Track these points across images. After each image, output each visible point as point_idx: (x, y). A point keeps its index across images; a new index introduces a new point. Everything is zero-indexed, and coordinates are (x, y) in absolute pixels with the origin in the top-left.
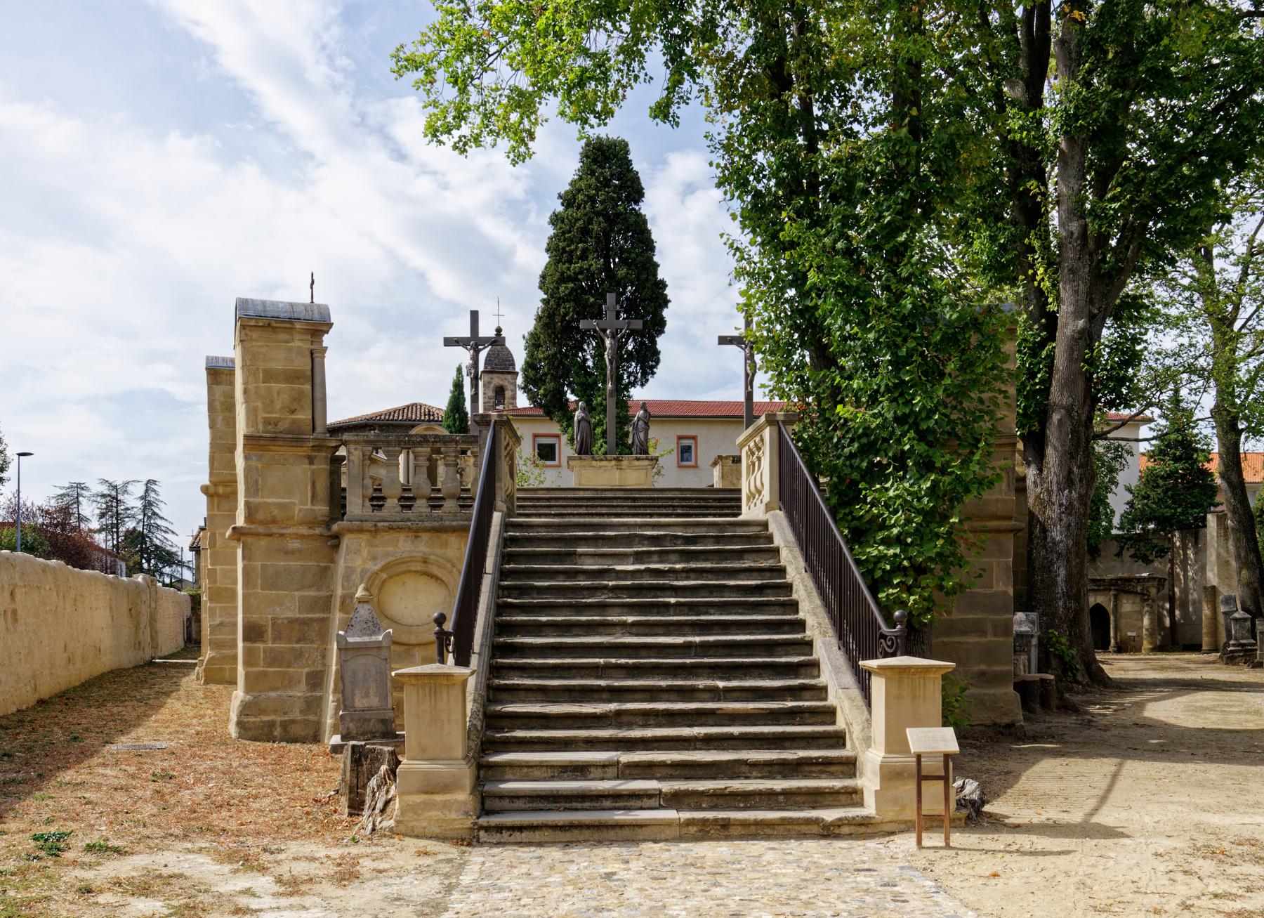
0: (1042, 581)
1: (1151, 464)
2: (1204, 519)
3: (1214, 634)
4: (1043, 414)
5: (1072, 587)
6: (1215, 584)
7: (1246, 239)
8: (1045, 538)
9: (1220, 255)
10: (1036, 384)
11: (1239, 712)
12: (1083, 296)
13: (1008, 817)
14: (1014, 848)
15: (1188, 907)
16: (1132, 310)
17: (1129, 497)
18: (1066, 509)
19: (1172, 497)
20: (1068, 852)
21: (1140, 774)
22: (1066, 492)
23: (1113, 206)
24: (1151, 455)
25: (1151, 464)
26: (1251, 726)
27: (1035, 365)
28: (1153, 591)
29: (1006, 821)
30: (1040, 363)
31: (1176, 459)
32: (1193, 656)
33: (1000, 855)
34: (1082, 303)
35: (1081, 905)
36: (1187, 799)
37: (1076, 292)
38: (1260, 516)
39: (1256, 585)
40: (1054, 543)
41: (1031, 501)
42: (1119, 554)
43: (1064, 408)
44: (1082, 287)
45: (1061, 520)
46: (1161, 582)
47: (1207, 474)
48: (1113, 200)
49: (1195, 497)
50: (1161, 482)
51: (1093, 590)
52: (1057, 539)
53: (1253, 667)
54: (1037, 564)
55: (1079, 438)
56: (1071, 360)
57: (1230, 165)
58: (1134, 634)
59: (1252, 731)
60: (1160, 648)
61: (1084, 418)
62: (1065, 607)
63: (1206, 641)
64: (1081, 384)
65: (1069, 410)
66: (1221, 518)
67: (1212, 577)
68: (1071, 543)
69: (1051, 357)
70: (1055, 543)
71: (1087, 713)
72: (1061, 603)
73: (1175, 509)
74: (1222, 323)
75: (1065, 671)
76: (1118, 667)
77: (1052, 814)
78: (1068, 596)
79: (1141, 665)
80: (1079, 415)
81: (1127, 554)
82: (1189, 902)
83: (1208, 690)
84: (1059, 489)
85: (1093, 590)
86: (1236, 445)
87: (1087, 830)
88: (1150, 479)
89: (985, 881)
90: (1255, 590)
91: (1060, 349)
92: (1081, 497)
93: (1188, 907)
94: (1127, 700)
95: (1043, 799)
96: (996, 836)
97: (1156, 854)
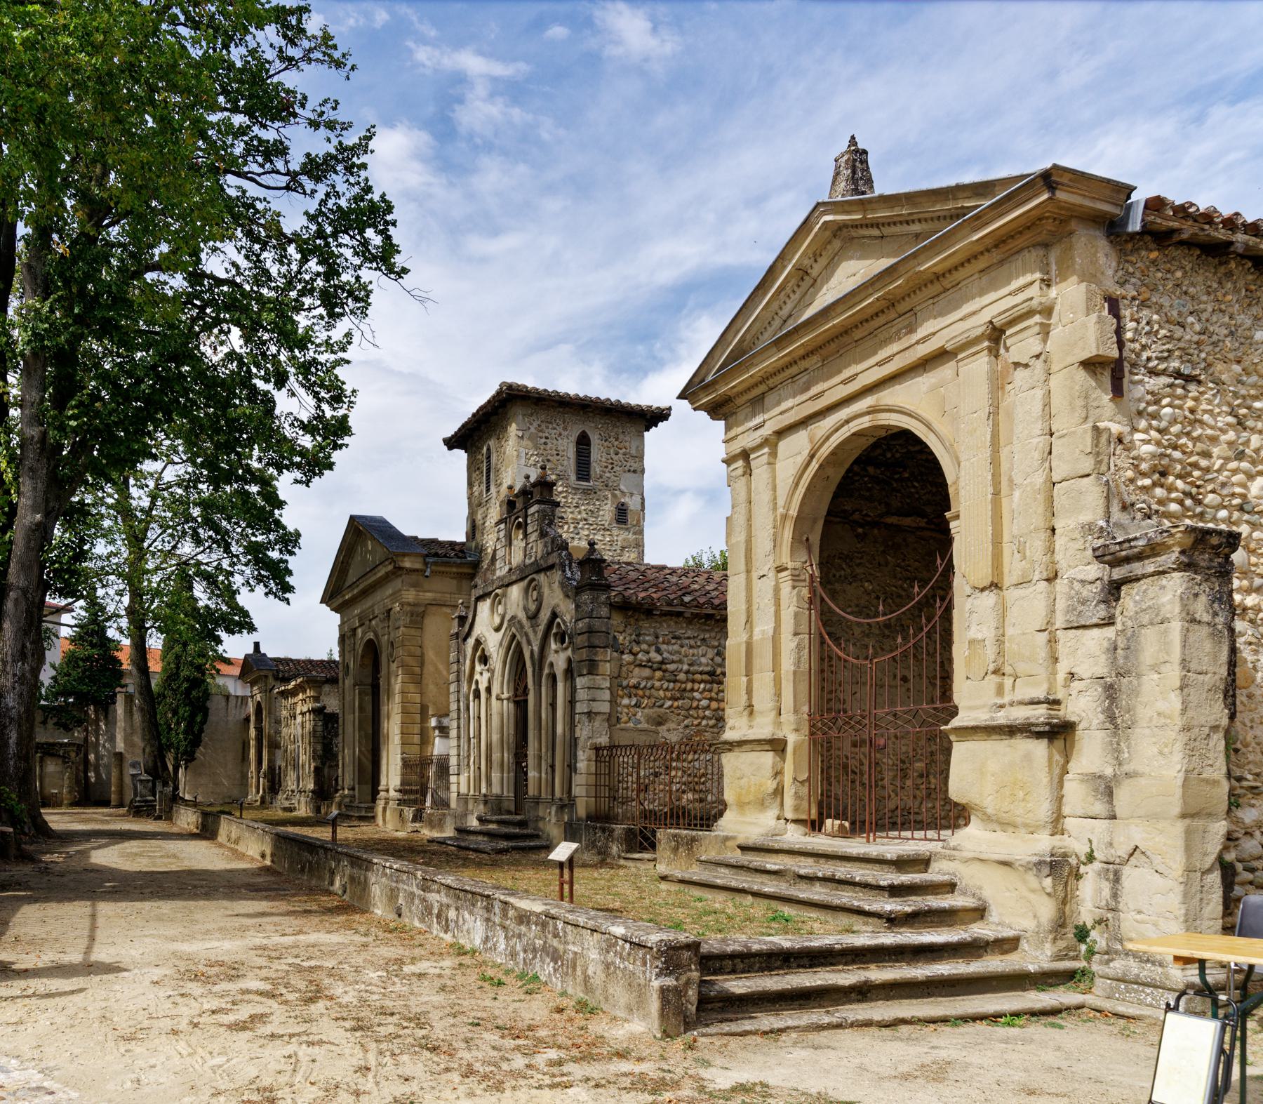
1: (72, 648)
3: (121, 791)
12: (40, 494)
13: (13, 963)
14: (30, 992)
15: (196, 1025)
16: (79, 516)
17: (54, 673)
20: (81, 990)
21: (110, 913)
24: (72, 640)
25: (72, 648)
28: (73, 755)
29: (14, 967)
31: (93, 646)
32: (105, 810)
33: (19, 1000)
34: (39, 500)
35: (109, 1036)
36: (155, 932)
37: (35, 489)
44: (40, 485)
46: (79, 747)
47: (117, 662)
50: (81, 663)
57: (160, 416)
60: (75, 804)
61: (37, 600)
62: (15, 767)
63: (114, 798)
65: (25, 592)
66: (129, 698)
67: (120, 746)
68: (22, 710)
71: (41, 861)
74: (136, 540)
76: (57, 820)
77: (47, 958)
79: (66, 818)
81: (51, 723)
82: (195, 1021)
84: (14, 661)
86: (143, 641)
87: (89, 968)
88: (71, 659)
89: (14, 1027)
93: (196, 1025)
94: (72, 849)
95: (35, 943)
96: (9, 983)
97: (153, 982)
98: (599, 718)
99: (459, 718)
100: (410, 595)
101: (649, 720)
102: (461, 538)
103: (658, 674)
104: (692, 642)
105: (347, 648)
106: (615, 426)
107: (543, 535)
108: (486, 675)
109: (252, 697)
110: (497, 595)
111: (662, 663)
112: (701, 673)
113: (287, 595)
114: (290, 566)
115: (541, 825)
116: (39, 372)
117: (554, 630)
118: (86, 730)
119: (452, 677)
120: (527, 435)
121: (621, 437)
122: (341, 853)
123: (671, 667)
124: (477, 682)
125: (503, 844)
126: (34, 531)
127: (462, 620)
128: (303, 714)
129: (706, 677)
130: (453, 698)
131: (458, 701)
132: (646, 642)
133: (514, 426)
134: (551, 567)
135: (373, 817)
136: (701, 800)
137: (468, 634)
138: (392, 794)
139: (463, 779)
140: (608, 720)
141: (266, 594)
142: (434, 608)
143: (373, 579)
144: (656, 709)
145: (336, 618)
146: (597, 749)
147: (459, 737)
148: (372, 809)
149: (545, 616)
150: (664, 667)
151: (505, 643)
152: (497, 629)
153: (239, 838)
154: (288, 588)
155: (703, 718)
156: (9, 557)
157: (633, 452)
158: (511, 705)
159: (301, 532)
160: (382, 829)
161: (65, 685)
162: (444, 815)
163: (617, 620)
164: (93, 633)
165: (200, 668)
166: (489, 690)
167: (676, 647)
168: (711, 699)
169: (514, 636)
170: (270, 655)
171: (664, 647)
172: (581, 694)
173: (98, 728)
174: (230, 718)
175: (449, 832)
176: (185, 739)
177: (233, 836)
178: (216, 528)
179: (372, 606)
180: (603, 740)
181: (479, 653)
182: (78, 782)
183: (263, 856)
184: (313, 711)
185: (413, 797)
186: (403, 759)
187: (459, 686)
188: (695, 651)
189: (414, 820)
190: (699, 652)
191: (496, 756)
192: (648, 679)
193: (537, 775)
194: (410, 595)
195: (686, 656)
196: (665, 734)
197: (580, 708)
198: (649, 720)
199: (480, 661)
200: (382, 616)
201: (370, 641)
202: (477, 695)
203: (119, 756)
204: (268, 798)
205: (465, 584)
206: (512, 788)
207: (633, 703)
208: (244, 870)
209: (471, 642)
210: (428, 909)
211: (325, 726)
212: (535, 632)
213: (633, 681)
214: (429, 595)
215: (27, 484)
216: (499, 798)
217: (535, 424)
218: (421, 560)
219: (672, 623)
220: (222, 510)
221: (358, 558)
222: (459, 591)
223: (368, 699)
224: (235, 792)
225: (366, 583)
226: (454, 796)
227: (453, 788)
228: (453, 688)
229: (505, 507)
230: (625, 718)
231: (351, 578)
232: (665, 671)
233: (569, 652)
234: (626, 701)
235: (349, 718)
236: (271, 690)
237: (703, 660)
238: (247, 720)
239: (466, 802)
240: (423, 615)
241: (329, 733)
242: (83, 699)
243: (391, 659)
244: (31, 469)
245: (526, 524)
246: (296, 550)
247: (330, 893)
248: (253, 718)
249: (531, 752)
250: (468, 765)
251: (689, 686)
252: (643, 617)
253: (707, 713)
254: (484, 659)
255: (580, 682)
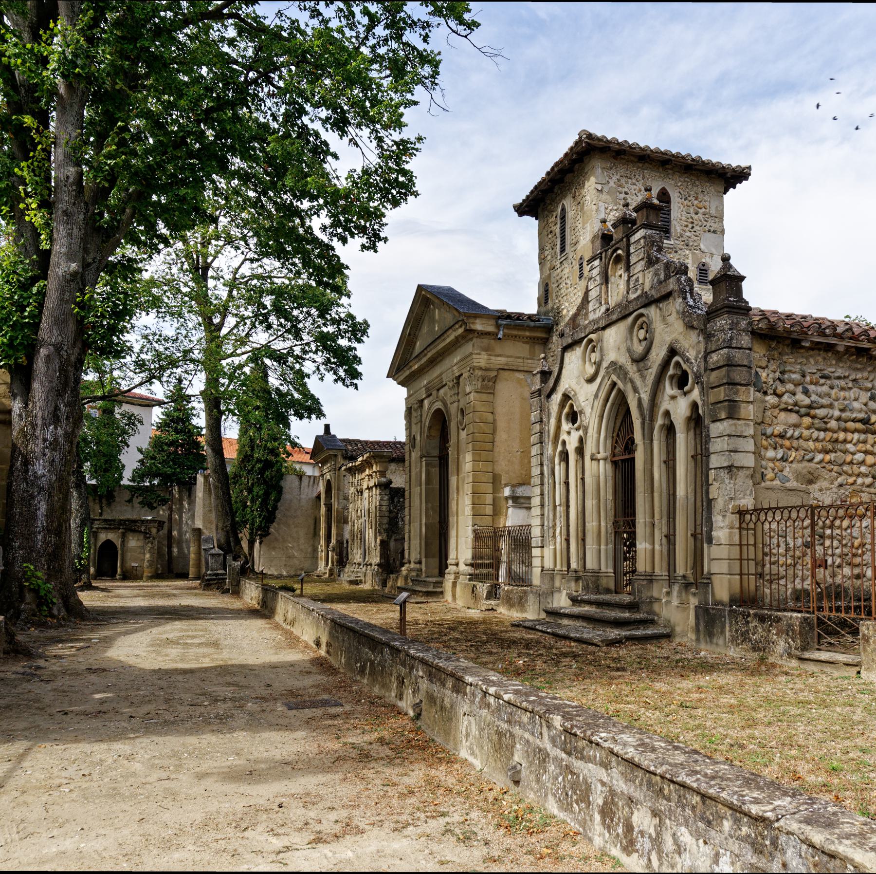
0: (21, 514)
1: (158, 433)
2: (195, 479)
4: (31, 349)
5: (52, 522)
6: (201, 527)
7: (231, 270)
8: (27, 471)
9: (212, 277)
10: (25, 317)
11: (200, 645)
17: (141, 457)
18: (51, 444)
19: (172, 460)
22: (51, 427)
23: (109, 162)
25: (158, 433)
26: (206, 663)
27: (25, 299)
28: (154, 531)
30: (30, 298)
31: (177, 432)
34: (75, 248)
37: (70, 235)
38: (234, 478)
39: (229, 528)
40: (36, 477)
41: (15, 433)
42: (130, 501)
43: (53, 345)
45: (44, 455)
46: (161, 524)
47: (197, 445)
48: (109, 156)
49: (190, 461)
50: (166, 448)
51: (105, 528)
52: (40, 473)
53: (223, 593)
54: (16, 497)
55: (67, 377)
56: (62, 300)
58: (136, 565)
59: (206, 670)
61: (73, 358)
62: (44, 541)
63: (192, 571)
64: (72, 326)
65: (58, 348)
66: (206, 478)
67: (199, 524)
68: (54, 478)
69: (42, 293)
70: (36, 477)
72: (40, 537)
73: (175, 469)
75: (39, 605)
78: (48, 530)
80: (68, 355)
81: (136, 501)
83: (179, 619)
84: (44, 424)
85: (105, 528)
88: (157, 443)
90: (227, 532)
91: (52, 285)
92: (66, 434)
98: (742, 474)
99: (542, 484)
100: (481, 360)
101: (798, 476)
102: (531, 307)
103: (807, 420)
104: (842, 383)
105: (414, 421)
106: (693, 185)
107: (651, 262)
108: (575, 435)
109: (322, 475)
110: (591, 341)
111: (810, 407)
112: (854, 420)
113: (355, 381)
114: (359, 353)
115: (656, 607)
116: (76, 108)
117: (671, 371)
118: (171, 509)
119: (534, 439)
120: (606, 189)
121: (701, 196)
122: (413, 658)
123: (821, 412)
124: (564, 443)
125: (614, 633)
126: (68, 282)
127: (545, 375)
128: (369, 489)
129: (859, 426)
130: (535, 461)
131: (542, 465)
132: (792, 381)
133: (593, 179)
134: (667, 296)
135: (442, 593)
136: (858, 577)
137: (553, 390)
138: (463, 568)
139: (548, 552)
140: (752, 476)
141: (336, 380)
142: (507, 373)
143: (443, 344)
144: (805, 464)
145: (403, 392)
146: (741, 513)
147: (542, 505)
148: (440, 584)
149: (658, 355)
150: (813, 412)
151: (602, 395)
152: (591, 380)
153: (295, 619)
154: (356, 375)
155: (858, 476)
156: (41, 312)
157: (713, 212)
158: (609, 466)
159: (370, 323)
160: (452, 605)
161: (150, 468)
162: (525, 592)
163: (759, 352)
164: (177, 420)
165: (274, 452)
166: (580, 451)
167: (825, 389)
168: (866, 452)
169: (614, 384)
170: (339, 436)
171: (812, 388)
172: (716, 445)
173: (181, 504)
174: (303, 496)
175: (531, 614)
176: (260, 516)
177: (290, 616)
178: (287, 316)
179: (441, 374)
180: (748, 502)
181: (566, 410)
182: (160, 554)
183: (318, 643)
184: (378, 485)
185: (485, 571)
186: (474, 531)
187: (542, 448)
188: (847, 394)
189: (489, 596)
190: (851, 394)
191: (591, 525)
192: (796, 426)
193: (649, 546)
194: (481, 360)
195: (837, 400)
196: (817, 495)
197: (715, 461)
198: (798, 476)
199: (567, 419)
200: (451, 384)
201: (438, 411)
202: (565, 456)
203: (198, 532)
204: (336, 570)
205: (538, 348)
206: (611, 563)
207: (779, 456)
208: (292, 665)
209: (557, 398)
210: (584, 793)
211: (391, 500)
212: (643, 377)
213: (778, 429)
214: (501, 360)
215: (61, 232)
216: (596, 573)
217: (615, 178)
218: (493, 322)
219: (820, 359)
220: (293, 298)
221: (425, 329)
222: (533, 356)
223: (435, 471)
224: (307, 565)
225: (434, 351)
226: (537, 571)
227: (536, 562)
228: (535, 450)
229: (598, 243)
230: (770, 475)
231: (419, 346)
232: (813, 417)
233: (696, 394)
234: (771, 453)
235: (416, 490)
236: (340, 468)
237: (856, 405)
238: (318, 497)
239: (552, 579)
240: (495, 379)
241: (395, 507)
242: (166, 479)
243: (461, 427)
244: (65, 213)
245: (628, 254)
246: (365, 338)
247: (400, 713)
248: (323, 496)
249: (641, 518)
250: (554, 536)
251: (842, 436)
252: (787, 350)
253: (863, 469)
254: (573, 417)
255: (716, 429)
